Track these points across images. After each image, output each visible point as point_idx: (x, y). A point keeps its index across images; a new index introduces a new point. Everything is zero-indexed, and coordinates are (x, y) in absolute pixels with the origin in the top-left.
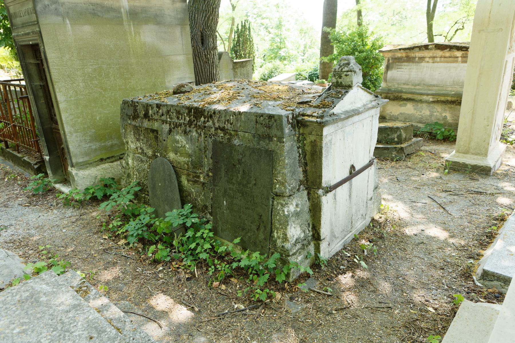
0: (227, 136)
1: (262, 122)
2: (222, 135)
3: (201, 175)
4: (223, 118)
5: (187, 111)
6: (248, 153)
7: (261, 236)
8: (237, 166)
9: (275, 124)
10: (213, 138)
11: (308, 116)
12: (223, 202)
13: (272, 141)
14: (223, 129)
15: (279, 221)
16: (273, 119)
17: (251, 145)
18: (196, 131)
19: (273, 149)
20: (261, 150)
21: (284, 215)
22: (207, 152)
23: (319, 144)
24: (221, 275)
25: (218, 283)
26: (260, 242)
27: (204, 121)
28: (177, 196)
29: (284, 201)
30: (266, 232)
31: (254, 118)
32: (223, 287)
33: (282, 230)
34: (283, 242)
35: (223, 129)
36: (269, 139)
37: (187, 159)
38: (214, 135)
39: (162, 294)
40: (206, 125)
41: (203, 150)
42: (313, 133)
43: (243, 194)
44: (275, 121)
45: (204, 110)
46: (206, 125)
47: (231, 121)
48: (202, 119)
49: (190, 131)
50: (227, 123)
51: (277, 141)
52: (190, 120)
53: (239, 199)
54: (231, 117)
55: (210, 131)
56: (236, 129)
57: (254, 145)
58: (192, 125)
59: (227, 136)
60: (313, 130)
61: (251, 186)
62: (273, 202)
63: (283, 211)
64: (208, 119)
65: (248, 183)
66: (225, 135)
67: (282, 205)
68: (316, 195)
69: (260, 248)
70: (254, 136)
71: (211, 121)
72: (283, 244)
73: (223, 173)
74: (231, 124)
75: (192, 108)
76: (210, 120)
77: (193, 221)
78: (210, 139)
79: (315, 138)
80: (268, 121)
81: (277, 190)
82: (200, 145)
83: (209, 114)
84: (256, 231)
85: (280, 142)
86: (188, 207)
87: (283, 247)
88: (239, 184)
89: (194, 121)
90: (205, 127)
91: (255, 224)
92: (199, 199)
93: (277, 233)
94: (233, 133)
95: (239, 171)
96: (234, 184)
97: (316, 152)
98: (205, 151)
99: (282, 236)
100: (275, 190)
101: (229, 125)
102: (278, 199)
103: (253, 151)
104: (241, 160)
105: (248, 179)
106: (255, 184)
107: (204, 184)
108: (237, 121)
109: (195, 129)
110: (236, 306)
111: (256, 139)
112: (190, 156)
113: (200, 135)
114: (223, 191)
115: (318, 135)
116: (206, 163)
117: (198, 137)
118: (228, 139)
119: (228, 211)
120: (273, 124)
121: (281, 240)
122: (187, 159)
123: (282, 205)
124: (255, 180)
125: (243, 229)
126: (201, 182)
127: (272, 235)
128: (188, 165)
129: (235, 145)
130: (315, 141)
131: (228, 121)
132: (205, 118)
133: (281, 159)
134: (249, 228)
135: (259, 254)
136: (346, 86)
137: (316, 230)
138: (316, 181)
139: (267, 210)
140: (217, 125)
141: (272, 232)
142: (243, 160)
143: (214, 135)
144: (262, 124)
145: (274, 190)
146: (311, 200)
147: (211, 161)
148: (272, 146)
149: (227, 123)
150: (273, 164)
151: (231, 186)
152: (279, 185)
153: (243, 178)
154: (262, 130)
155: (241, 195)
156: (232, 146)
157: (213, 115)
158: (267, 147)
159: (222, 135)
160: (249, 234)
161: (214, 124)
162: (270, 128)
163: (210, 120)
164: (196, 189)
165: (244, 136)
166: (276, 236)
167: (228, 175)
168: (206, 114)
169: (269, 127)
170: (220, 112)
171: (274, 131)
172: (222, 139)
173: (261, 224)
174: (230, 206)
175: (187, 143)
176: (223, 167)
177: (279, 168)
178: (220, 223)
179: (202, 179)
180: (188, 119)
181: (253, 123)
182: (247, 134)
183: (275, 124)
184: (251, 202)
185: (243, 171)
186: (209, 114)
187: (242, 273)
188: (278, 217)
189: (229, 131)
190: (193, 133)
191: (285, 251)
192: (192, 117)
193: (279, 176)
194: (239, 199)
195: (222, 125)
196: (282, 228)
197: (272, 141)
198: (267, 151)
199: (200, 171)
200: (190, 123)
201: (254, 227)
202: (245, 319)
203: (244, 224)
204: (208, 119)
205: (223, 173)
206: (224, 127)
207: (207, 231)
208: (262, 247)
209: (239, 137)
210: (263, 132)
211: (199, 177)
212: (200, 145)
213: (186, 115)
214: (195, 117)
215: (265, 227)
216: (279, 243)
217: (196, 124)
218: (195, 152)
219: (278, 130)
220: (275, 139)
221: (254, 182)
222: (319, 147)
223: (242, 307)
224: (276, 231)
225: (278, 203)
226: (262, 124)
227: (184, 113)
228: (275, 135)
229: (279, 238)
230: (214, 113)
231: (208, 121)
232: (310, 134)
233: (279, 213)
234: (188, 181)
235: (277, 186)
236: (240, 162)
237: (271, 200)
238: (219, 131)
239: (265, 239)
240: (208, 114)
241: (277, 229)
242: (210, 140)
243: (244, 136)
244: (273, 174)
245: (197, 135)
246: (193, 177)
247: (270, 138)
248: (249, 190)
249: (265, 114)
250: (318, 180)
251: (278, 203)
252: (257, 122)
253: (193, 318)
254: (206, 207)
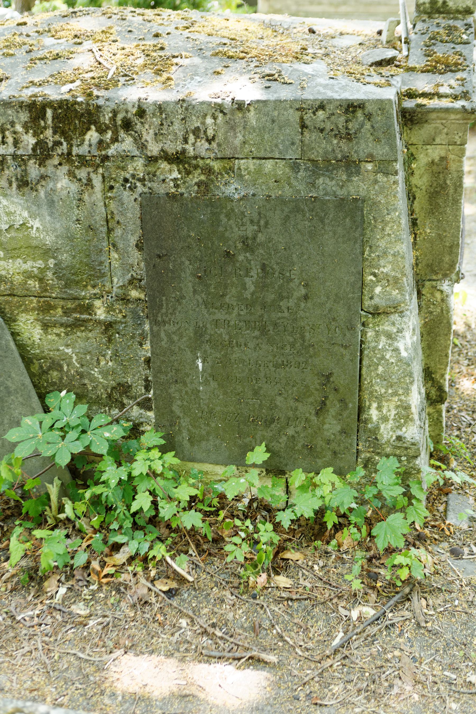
0: (197, 176)
1: (322, 125)
2: (176, 175)
3: (98, 303)
4: (177, 126)
5: (24, 116)
6: (276, 218)
7: (331, 427)
8: (241, 258)
9: (368, 126)
10: (140, 188)
11: (424, 95)
12: (194, 362)
13: (358, 173)
14: (178, 159)
15: (383, 378)
16: (359, 114)
17: (288, 192)
18: (71, 174)
19: (363, 193)
20: (324, 203)
21: (400, 360)
22: (118, 232)
23: (453, 167)
24: (266, 553)
25: (264, 576)
26: (328, 442)
27: (101, 142)
28: (20, 376)
29: (393, 324)
30: (345, 414)
31: (294, 116)
32: (282, 580)
33: (396, 399)
34: (399, 427)
35: (178, 159)
36: (347, 169)
37: (40, 264)
38: (142, 180)
39: (130, 655)
40: (111, 151)
41: (104, 229)
42: (438, 140)
43: (264, 331)
44: (369, 117)
45: (99, 107)
46: (111, 151)
47: (210, 133)
48: (92, 135)
49: (43, 177)
50: (192, 138)
51: (376, 172)
52: (40, 144)
53: (251, 345)
54: (209, 121)
55: (124, 169)
56: (228, 153)
57: (298, 191)
58: (49, 157)
59: (197, 176)
60: (438, 132)
61: (291, 303)
62: (364, 333)
63: (396, 350)
64: (116, 133)
65: (281, 298)
66: (188, 173)
67: (389, 336)
68: (438, 295)
69: (329, 455)
70: (295, 167)
71: (129, 140)
72: (399, 433)
73: (188, 283)
74: (209, 141)
75: (44, 107)
76: (122, 134)
77: (107, 435)
78: (126, 193)
79: (443, 154)
80: (343, 119)
81: (376, 301)
82: (91, 215)
83: (120, 117)
84: (314, 418)
85: (386, 174)
86: (63, 399)
87: (399, 438)
88: (250, 305)
89: (58, 144)
90: (106, 158)
91: (311, 400)
92: (96, 372)
93: (379, 408)
94: (216, 166)
95: (248, 271)
96: (229, 307)
97: (444, 187)
98: (110, 231)
99: (393, 412)
100: (373, 302)
101: (203, 145)
102: (375, 325)
103: (295, 207)
104: (254, 238)
105: (281, 287)
106: (306, 297)
107: (109, 326)
108: (233, 128)
109: (65, 168)
110: (355, 614)
111: (302, 174)
112: (47, 253)
113: (89, 182)
114: (191, 332)
115: (455, 144)
116: (115, 264)
117: (81, 193)
118: (199, 184)
119: (213, 384)
120: (362, 126)
121: (391, 423)
122: (40, 264)
123: (389, 336)
124: (306, 286)
125: (269, 422)
126: (99, 322)
127: (364, 416)
128: (41, 280)
129: (229, 199)
130: (442, 159)
131: (196, 132)
132: (101, 131)
133: (388, 218)
134: (290, 414)
135: (334, 472)
136: (458, 12)
137: (432, 379)
138: (441, 261)
139: (347, 357)
140: (154, 149)
141: (361, 410)
142: (261, 238)
143: (142, 180)
144: (322, 130)
145: (367, 303)
146: (424, 310)
147: (136, 256)
148: (358, 187)
149: (192, 138)
150: (363, 235)
151: (220, 315)
152: (383, 287)
153: (262, 286)
154: (321, 147)
155: (257, 333)
156: (219, 206)
157: (135, 120)
158: (341, 193)
159: (176, 175)
160: (290, 431)
161: (143, 147)
162: (350, 140)
163: (122, 134)
164: (81, 344)
165: (259, 171)
166: (375, 418)
167: (208, 286)
168: (106, 118)
169: (349, 137)
170: (161, 108)
171: (365, 146)
172: (176, 186)
173: (331, 397)
174: (220, 373)
175: (33, 216)
176: (188, 268)
177: (382, 244)
178: (185, 422)
179: (101, 313)
180: (30, 140)
181: (293, 131)
182: (269, 165)
183: (368, 126)
184: (293, 345)
185: (264, 267)
186: (120, 117)
187: (314, 530)
188: (381, 369)
189: (201, 162)
190: (56, 181)
191: (406, 448)
192: (49, 132)
193: (382, 262)
194: (251, 345)
195: (173, 147)
196: (395, 394)
197: (358, 173)
198: (342, 203)
199: (96, 291)
200: (42, 153)
201: (306, 409)
202: (401, 635)
203: (273, 407)
204: (116, 133)
205: (188, 283)
206: (184, 151)
207: (156, 453)
208: (335, 453)
209: (241, 176)
210: (326, 153)
211: (89, 309)
212: (91, 215)
213: (19, 128)
214: (63, 133)
215: (341, 401)
216: (386, 433)
217: (69, 154)
218: (71, 238)
219: (377, 140)
220: (369, 167)
221: (303, 291)
222: (455, 175)
223: (369, 612)
224: (375, 405)
225: (377, 334)
226: (322, 130)
227: (13, 124)
228: (371, 155)
229: (385, 419)
230: (141, 113)
231: (115, 140)
232: (430, 142)
233: (383, 358)
234: (46, 326)
235: (378, 290)
236: (248, 244)
237: (360, 327)
238: (164, 165)
239: (343, 432)
240: (113, 119)
241: (380, 399)
242: (127, 197)
243: (259, 171)
244: (364, 260)
245: (74, 187)
246: (66, 312)
247: (351, 165)
248: (286, 314)
249: (330, 101)
250: (447, 259)
251: (377, 334)
252: (303, 126)
253: (276, 685)
254: (124, 389)
